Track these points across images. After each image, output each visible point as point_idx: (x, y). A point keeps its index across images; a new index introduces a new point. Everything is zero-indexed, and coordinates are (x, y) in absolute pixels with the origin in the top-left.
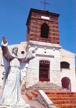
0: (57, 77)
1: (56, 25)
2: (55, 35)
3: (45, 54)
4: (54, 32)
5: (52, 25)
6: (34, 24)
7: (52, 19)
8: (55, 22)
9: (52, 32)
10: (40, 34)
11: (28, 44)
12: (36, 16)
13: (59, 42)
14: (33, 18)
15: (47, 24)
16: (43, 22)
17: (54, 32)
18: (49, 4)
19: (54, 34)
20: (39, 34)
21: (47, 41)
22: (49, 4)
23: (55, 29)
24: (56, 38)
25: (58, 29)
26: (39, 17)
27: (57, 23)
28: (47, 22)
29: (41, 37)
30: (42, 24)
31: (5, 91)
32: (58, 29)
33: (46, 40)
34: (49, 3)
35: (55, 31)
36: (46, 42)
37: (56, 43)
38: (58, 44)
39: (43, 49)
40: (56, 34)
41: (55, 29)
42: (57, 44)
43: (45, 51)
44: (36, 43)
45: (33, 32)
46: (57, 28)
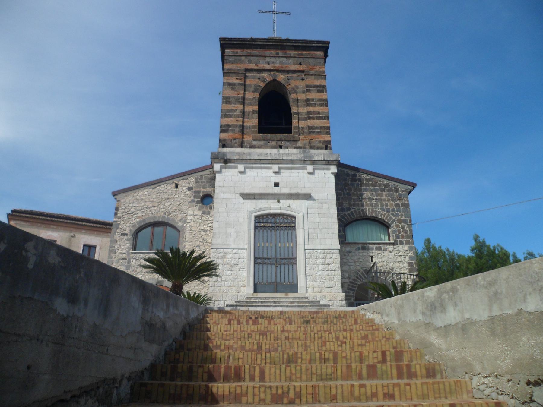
0: (326, 273)
1: (318, 82)
2: (313, 118)
3: (276, 190)
4: (311, 109)
5: (301, 84)
6: (233, 89)
7: (300, 64)
8: (311, 72)
9: (304, 110)
10: (256, 121)
11: (111, 241)
12: (242, 62)
13: (329, 143)
14: (228, 69)
15: (283, 82)
16: (268, 77)
17: (311, 109)
18: (288, 13)
19: (310, 116)
20: (253, 122)
21: (283, 144)
22: (288, 13)
23: (314, 95)
24: (317, 128)
25: (323, 96)
26: (250, 62)
27: (323, 76)
28: (281, 78)
29: (260, 131)
30: (262, 85)
31: (274, 136)
32: (323, 96)
33: (281, 140)
34: (382, 215)
35: (315, 105)
36: (281, 147)
37: (318, 148)
38: (326, 148)
39: (270, 173)
40: (319, 113)
41: (314, 95)
42: (322, 148)
43: (276, 179)
44: (239, 154)
45: (231, 116)
46: (322, 91)
